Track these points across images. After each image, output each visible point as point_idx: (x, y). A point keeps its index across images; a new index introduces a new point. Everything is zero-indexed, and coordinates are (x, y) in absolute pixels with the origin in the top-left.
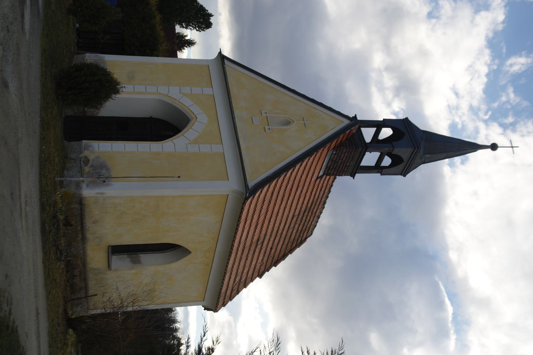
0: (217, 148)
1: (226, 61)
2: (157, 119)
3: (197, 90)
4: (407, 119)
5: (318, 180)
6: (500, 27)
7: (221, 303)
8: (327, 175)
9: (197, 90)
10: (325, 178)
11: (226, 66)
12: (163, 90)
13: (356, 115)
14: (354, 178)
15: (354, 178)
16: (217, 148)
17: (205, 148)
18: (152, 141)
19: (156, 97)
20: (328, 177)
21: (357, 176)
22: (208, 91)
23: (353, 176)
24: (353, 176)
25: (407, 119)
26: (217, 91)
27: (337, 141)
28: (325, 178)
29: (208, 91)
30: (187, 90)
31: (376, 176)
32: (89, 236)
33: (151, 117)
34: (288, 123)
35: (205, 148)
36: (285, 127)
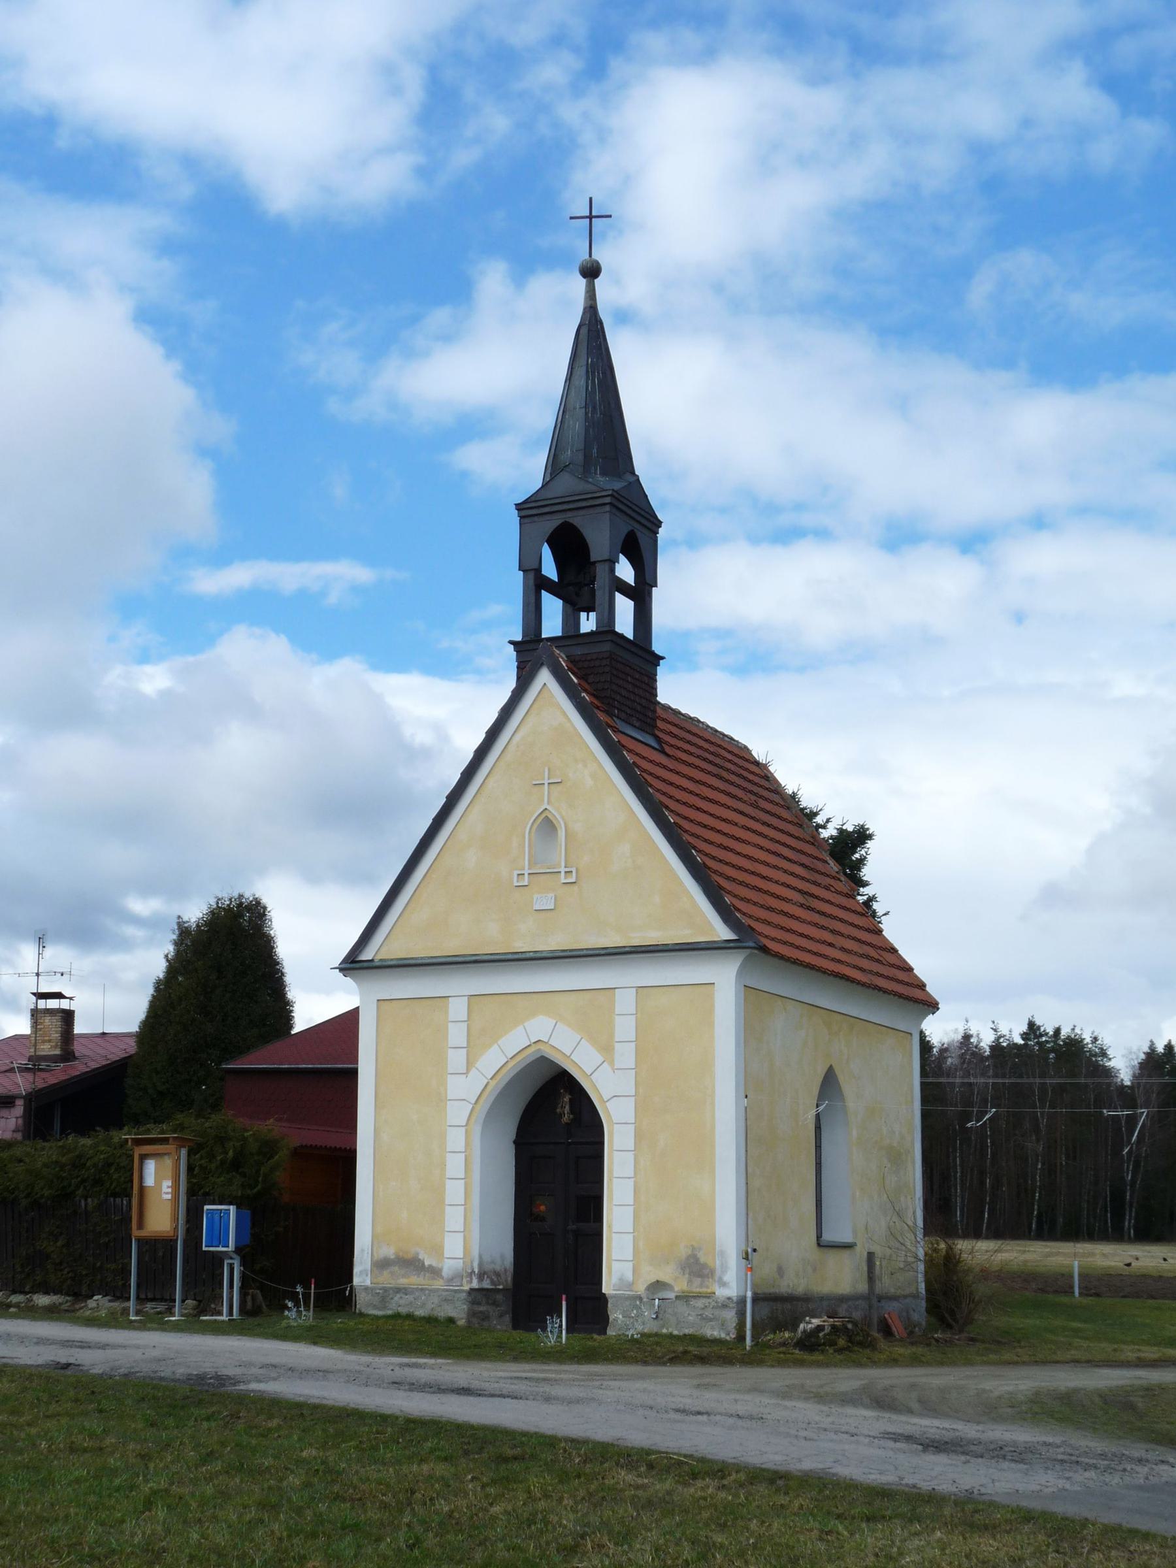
0: (625, 1002)
1: (367, 955)
2: (519, 1129)
3: (457, 1035)
4: (519, 507)
5: (668, 749)
6: (1137, 1072)
7: (917, 993)
8: (655, 726)
9: (457, 1035)
10: (661, 730)
11: (383, 955)
12: (458, 1114)
13: (511, 642)
14: (663, 658)
15: (663, 658)
16: (625, 1002)
17: (625, 1028)
18: (601, 1143)
19: (477, 1130)
20: (659, 723)
21: (657, 647)
22: (458, 1009)
23: (657, 659)
24: (657, 659)
25: (519, 507)
26: (458, 989)
27: (598, 708)
28: (661, 730)
29: (458, 1009)
30: (456, 1059)
31: (659, 597)
32: (800, 1290)
33: (515, 1142)
34: (547, 826)
35: (625, 1028)
36: (562, 834)
